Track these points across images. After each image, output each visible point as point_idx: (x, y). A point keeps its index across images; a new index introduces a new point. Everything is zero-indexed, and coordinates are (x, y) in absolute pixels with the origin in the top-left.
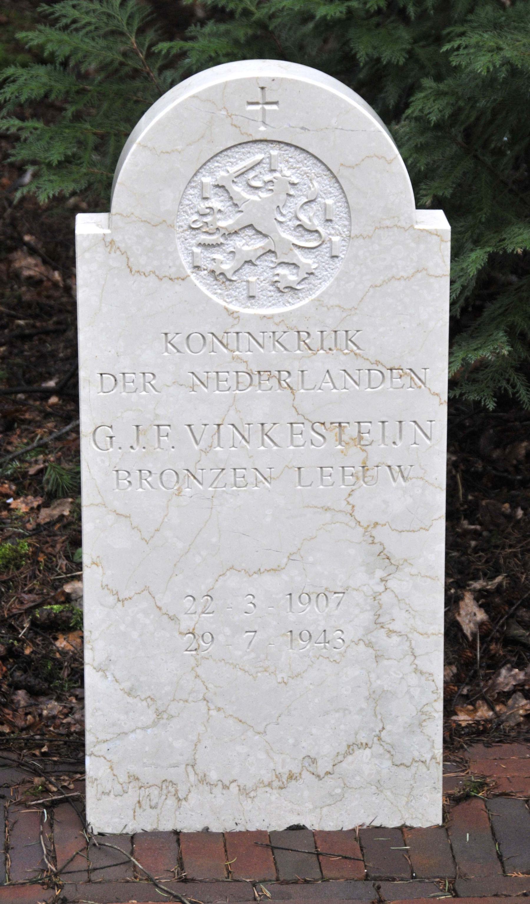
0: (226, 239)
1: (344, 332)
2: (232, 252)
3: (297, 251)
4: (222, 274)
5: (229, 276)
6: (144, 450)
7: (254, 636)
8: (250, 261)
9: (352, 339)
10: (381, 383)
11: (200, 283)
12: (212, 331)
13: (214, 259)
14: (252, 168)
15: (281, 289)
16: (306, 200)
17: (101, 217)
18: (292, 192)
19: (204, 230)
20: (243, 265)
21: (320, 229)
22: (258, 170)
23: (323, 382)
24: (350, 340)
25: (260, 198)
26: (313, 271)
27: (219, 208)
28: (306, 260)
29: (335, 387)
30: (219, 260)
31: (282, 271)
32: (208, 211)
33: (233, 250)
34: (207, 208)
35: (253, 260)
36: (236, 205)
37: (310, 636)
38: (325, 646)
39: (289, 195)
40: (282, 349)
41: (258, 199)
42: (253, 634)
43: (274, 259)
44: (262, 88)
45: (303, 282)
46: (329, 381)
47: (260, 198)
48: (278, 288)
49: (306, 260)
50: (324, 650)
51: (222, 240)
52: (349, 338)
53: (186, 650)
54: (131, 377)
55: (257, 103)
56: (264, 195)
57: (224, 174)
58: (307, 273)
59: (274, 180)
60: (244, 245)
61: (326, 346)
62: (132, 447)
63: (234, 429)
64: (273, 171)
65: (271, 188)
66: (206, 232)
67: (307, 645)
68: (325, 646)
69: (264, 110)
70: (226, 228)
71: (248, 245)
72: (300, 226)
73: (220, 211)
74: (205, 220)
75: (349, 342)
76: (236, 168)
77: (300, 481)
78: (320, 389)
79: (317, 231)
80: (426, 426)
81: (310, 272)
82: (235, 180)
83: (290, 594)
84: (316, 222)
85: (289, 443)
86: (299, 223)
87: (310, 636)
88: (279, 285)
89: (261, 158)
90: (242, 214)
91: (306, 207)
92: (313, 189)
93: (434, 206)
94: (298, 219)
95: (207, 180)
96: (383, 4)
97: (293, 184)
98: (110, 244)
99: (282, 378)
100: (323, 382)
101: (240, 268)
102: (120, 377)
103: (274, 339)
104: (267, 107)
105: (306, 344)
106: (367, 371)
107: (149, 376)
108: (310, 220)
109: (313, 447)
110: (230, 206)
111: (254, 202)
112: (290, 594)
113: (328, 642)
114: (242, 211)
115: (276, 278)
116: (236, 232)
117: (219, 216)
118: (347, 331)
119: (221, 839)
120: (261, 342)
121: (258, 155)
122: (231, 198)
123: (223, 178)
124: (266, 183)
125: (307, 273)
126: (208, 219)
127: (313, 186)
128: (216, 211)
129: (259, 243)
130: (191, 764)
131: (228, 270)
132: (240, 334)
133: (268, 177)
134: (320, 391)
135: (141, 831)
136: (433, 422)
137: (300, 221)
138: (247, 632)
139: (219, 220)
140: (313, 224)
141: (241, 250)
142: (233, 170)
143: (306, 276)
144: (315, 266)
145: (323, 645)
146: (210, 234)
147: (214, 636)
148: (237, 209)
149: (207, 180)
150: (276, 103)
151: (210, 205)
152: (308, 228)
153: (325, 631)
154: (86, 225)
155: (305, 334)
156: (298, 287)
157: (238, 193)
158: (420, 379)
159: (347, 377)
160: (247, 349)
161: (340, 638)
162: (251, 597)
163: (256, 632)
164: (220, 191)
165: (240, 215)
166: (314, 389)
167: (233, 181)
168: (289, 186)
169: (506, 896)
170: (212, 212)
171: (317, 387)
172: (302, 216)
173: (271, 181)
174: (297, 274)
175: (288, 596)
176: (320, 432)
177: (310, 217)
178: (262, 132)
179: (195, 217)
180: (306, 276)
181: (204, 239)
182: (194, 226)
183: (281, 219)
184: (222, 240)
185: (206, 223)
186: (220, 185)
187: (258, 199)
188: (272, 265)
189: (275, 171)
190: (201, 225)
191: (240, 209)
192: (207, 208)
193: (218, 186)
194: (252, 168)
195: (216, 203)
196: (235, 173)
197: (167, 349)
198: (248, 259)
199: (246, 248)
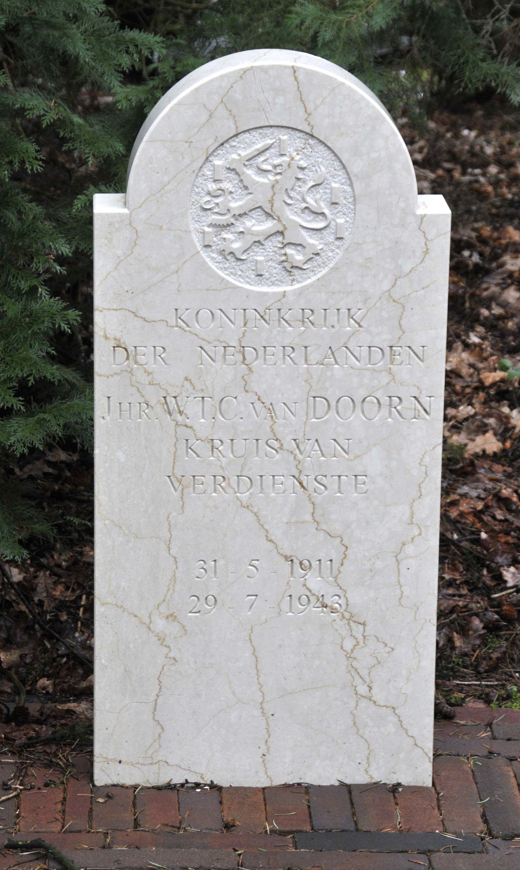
0: (237, 220)
2: (242, 232)
3: (304, 233)
4: (231, 253)
7: (255, 600)
8: (259, 242)
11: (211, 260)
16: (314, 184)
18: (300, 176)
21: (326, 211)
22: (267, 154)
25: (269, 180)
26: (319, 251)
27: (230, 189)
29: (337, 363)
30: (230, 239)
31: (289, 251)
32: (220, 192)
33: (242, 230)
35: (262, 241)
36: (246, 188)
37: (216, 600)
39: (298, 179)
40: (195, 455)
42: (254, 597)
45: (309, 262)
46: (318, 449)
47: (269, 180)
50: (322, 614)
51: (232, 220)
52: (179, 316)
53: (190, 612)
57: (235, 156)
58: (313, 254)
60: (253, 225)
64: (282, 155)
67: (212, 609)
68: (323, 610)
71: (262, 226)
72: (306, 208)
73: (231, 193)
74: (217, 201)
75: (179, 320)
76: (249, 151)
77: (257, 452)
79: (323, 214)
80: (425, 400)
82: (247, 163)
84: (322, 204)
86: (304, 205)
87: (216, 600)
91: (312, 189)
93: (434, 192)
94: (304, 200)
95: (217, 162)
96: (220, 2)
97: (302, 169)
98: (129, 222)
105: (310, 322)
107: (159, 349)
111: (264, 183)
114: (251, 193)
115: (284, 258)
119: (261, 794)
120: (232, 318)
122: (241, 181)
124: (275, 167)
125: (313, 254)
127: (321, 171)
129: (268, 225)
130: (496, 734)
131: (238, 249)
136: (432, 398)
137: (307, 203)
138: (248, 596)
140: (320, 207)
143: (312, 256)
145: (320, 609)
149: (217, 162)
152: (313, 209)
161: (202, 568)
162: (337, 597)
163: (256, 595)
165: (250, 196)
167: (244, 164)
168: (298, 170)
169: (167, 825)
172: (308, 199)
179: (208, 198)
180: (312, 256)
181: (213, 219)
183: (289, 201)
184: (232, 220)
190: (213, 205)
193: (229, 169)
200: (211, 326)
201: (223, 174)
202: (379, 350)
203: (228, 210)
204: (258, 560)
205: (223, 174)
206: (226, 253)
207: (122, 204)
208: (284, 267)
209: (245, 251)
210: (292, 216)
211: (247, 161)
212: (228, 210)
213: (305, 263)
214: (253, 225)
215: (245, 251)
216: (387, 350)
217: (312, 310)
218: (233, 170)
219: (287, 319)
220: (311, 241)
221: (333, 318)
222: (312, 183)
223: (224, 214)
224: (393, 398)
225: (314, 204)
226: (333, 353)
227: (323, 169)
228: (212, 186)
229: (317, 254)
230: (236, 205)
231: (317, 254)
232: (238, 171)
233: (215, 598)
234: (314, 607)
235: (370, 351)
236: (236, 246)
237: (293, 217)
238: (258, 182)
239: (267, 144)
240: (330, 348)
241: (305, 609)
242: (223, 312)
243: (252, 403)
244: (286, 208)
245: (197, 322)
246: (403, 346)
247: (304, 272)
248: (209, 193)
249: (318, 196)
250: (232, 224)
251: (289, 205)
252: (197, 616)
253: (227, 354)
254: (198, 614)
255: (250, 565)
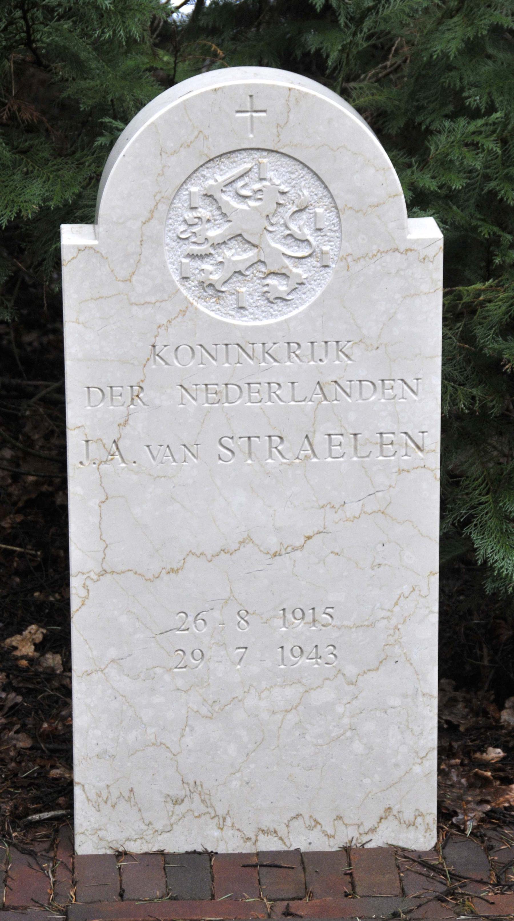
1: (335, 343)
2: (221, 263)
3: (287, 261)
5: (218, 287)
6: (134, 465)
7: (245, 652)
9: (269, 352)
10: (239, 398)
12: (238, 342)
13: (203, 270)
14: (242, 176)
15: (271, 299)
16: (297, 209)
17: (86, 228)
19: (193, 240)
20: (233, 275)
21: (311, 239)
22: (246, 179)
23: (313, 394)
24: (267, 353)
25: (249, 206)
26: (304, 281)
28: (300, 271)
30: (208, 270)
31: (272, 281)
34: (195, 218)
37: (203, 655)
38: (317, 661)
39: (278, 204)
41: (247, 208)
42: (244, 650)
43: (263, 269)
44: (251, 96)
47: (249, 206)
48: (268, 299)
49: (300, 271)
50: (316, 666)
52: (157, 353)
53: (176, 668)
54: (390, 384)
55: (247, 112)
56: (252, 203)
57: (211, 182)
58: (298, 284)
59: (264, 189)
60: (233, 255)
61: (317, 358)
62: (81, 463)
63: (407, 438)
64: (262, 179)
65: (259, 197)
66: (194, 243)
67: (199, 664)
68: (317, 661)
69: (252, 117)
70: (213, 238)
71: (238, 256)
72: (289, 235)
75: (266, 355)
78: (310, 400)
79: (307, 240)
81: (300, 282)
82: (224, 189)
83: (313, 609)
85: (328, 454)
86: (288, 232)
87: (203, 655)
88: (269, 295)
89: (250, 167)
90: (230, 224)
92: (302, 198)
94: (287, 228)
95: (194, 189)
97: (283, 193)
99: (273, 390)
100: (313, 394)
101: (230, 278)
102: (107, 390)
103: (154, 354)
104: (255, 114)
106: (358, 382)
107: (274, 386)
108: (300, 228)
109: (221, 462)
110: (220, 215)
111: (242, 211)
112: (313, 609)
113: (320, 658)
115: (266, 289)
116: (224, 243)
117: (208, 226)
118: (264, 344)
121: (245, 163)
123: (211, 186)
124: (255, 192)
125: (298, 284)
126: (195, 229)
127: (303, 195)
128: (204, 220)
129: (251, 254)
132: (229, 346)
133: (257, 186)
134: (310, 403)
135: (386, 846)
136: (426, 434)
137: (290, 230)
139: (207, 230)
140: (304, 234)
141: (229, 260)
142: (220, 179)
143: (297, 286)
144: (304, 276)
145: (314, 660)
146: (199, 244)
147: (204, 653)
148: (225, 219)
149: (194, 189)
150: (265, 111)
151: (199, 215)
153: (316, 646)
154: (71, 235)
155: (295, 345)
156: (290, 297)
157: (227, 203)
158: (191, 396)
159: (405, 387)
160: (200, 362)
161: (332, 653)
162: (332, 648)
163: (246, 648)
164: (208, 201)
166: (304, 400)
167: (222, 190)
168: (278, 194)
170: (200, 223)
171: (307, 400)
172: (294, 227)
173: (260, 190)
174: (287, 285)
175: (280, 649)
176: (228, 447)
177: (301, 226)
178: (252, 140)
179: (183, 228)
180: (297, 286)
181: (192, 250)
182: (183, 236)
183: (270, 228)
185: (194, 233)
186: (209, 194)
187: (247, 208)
188: (261, 275)
189: (264, 179)
190: (190, 235)
191: (228, 219)
192: (195, 218)
194: (242, 176)
195: (204, 212)
196: (223, 182)
197: (264, 360)
198: (237, 270)
199: (236, 258)
200: (190, 364)
201: (198, 202)
202: (99, 391)
203: (206, 239)
204: (332, 608)
205: (198, 202)
206: (205, 285)
207: (93, 236)
208: (268, 299)
209: (226, 282)
210: (275, 244)
211: (225, 186)
212: (206, 239)
213: (288, 294)
214: (233, 255)
215: (226, 282)
216: (107, 390)
217: (298, 344)
218: (211, 196)
219: (347, 353)
220: (295, 270)
221: (320, 352)
222: (295, 209)
223: (203, 243)
224: (273, 438)
225: (297, 231)
226: (321, 389)
227: (306, 192)
228: (189, 215)
229: (302, 284)
230: (214, 233)
231: (302, 284)
232: (215, 197)
233: (300, 648)
234: (307, 658)
235: (89, 392)
236: (214, 277)
237: (274, 245)
238: (236, 210)
239: (245, 168)
240: (318, 383)
241: (298, 661)
242: (241, 348)
243: (148, 446)
244: (268, 236)
245: (177, 358)
246: (396, 379)
247: (289, 302)
248: (185, 221)
249: (301, 223)
250: (211, 254)
251: (271, 232)
252: (183, 672)
253: (114, 394)
254: (184, 670)
255: (324, 613)
